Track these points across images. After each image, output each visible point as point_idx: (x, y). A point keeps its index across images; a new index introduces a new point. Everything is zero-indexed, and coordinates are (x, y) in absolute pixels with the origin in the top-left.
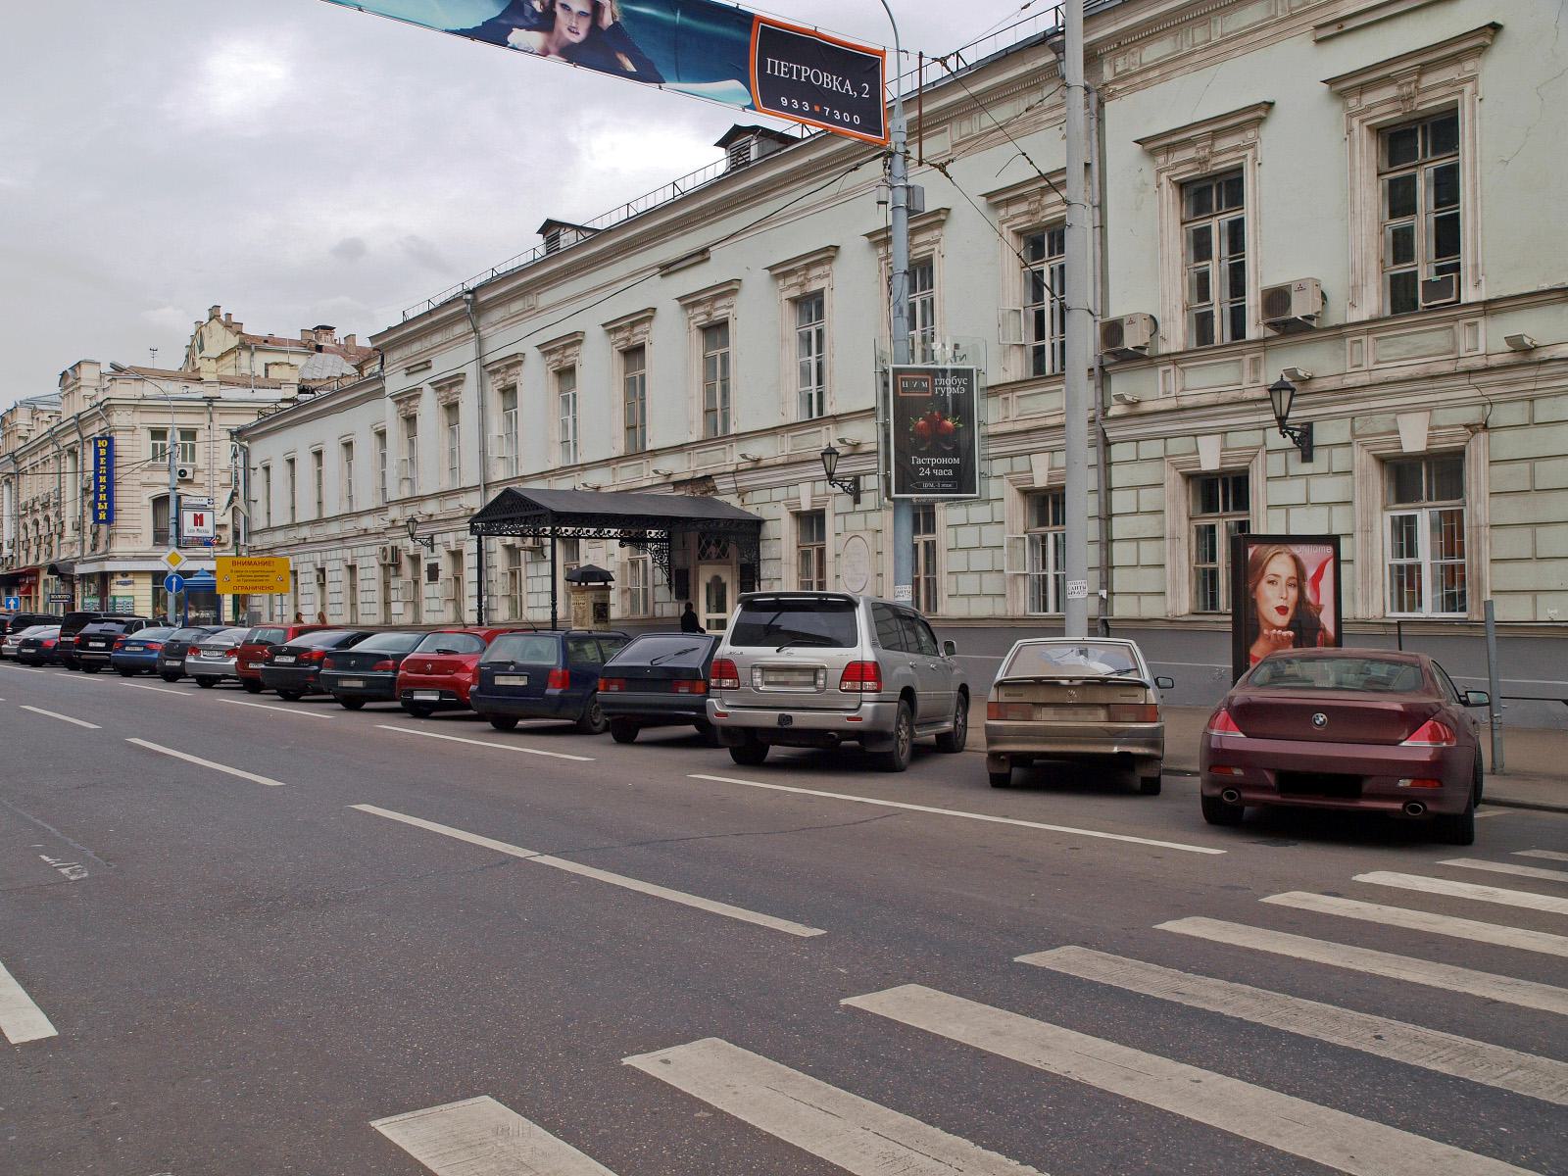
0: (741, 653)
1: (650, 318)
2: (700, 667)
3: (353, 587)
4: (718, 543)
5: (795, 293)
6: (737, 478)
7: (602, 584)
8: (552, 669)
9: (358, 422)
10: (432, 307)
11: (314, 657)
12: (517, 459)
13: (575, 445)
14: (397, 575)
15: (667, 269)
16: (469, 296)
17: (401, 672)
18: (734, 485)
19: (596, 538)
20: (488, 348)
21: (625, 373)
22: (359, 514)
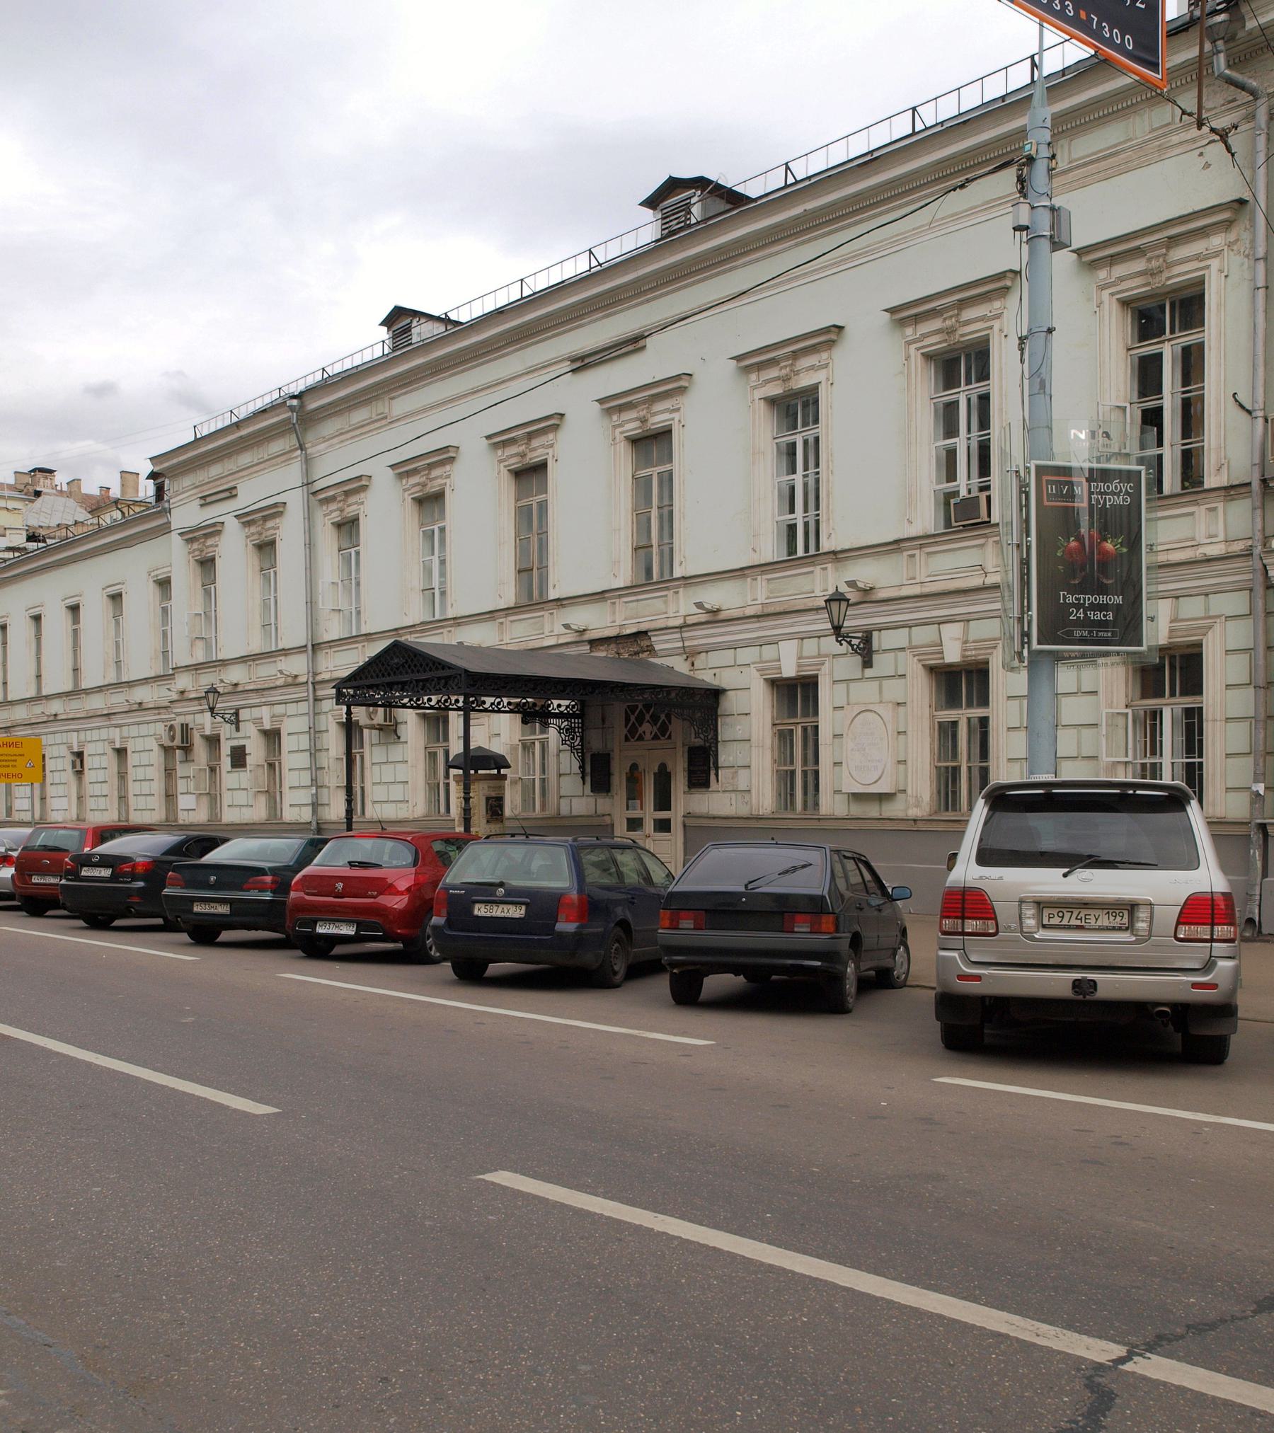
0: (1001, 878)
1: (555, 428)
2: (826, 893)
3: (122, 776)
4: (654, 719)
5: (775, 390)
6: (684, 635)
7: (495, 772)
8: (562, 895)
9: (132, 568)
10: (235, 419)
11: (140, 869)
12: (359, 613)
13: (443, 593)
14: (186, 760)
15: (583, 363)
16: (295, 402)
17: (293, 894)
18: (680, 644)
19: (493, 711)
20: (318, 472)
21: (517, 500)
22: (130, 684)
